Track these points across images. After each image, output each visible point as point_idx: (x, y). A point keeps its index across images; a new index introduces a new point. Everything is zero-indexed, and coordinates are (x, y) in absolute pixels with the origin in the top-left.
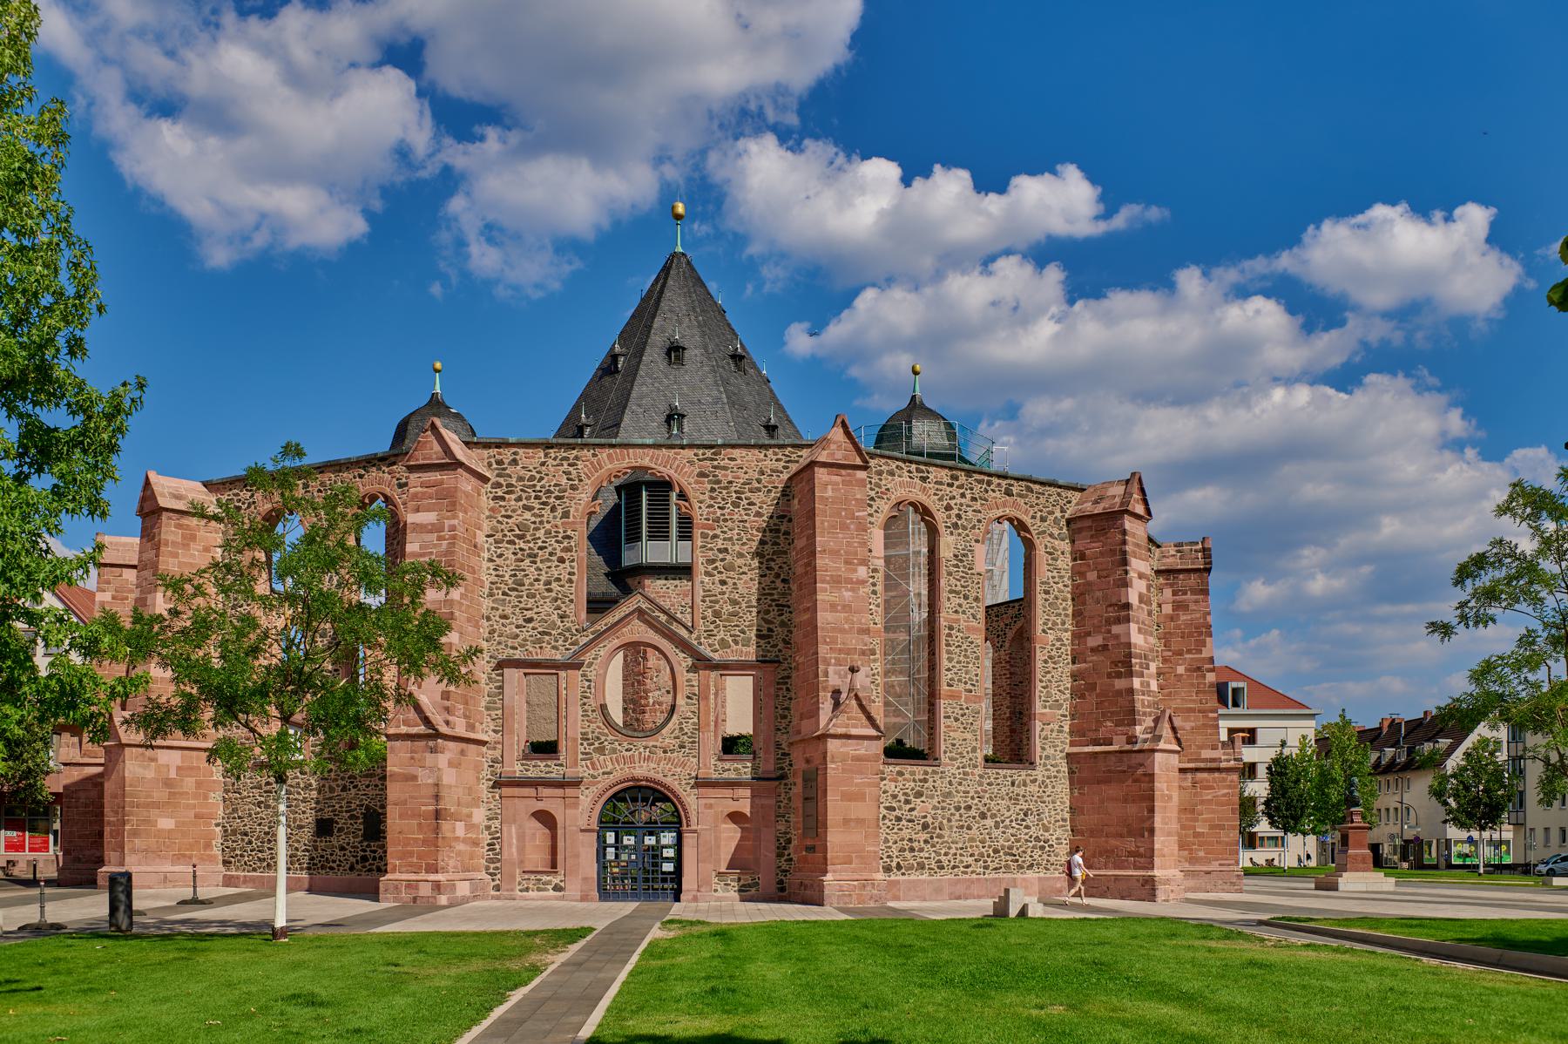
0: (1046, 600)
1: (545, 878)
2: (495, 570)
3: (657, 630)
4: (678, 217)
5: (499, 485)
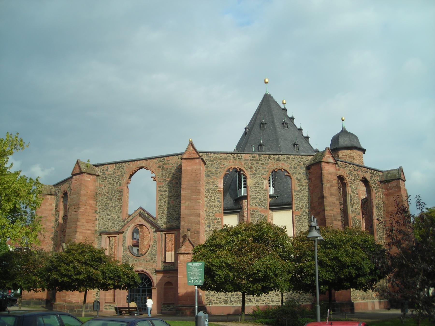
0: (298, 198)
1: (112, 305)
2: (101, 204)
3: (145, 220)
4: (266, 83)
5: (103, 177)
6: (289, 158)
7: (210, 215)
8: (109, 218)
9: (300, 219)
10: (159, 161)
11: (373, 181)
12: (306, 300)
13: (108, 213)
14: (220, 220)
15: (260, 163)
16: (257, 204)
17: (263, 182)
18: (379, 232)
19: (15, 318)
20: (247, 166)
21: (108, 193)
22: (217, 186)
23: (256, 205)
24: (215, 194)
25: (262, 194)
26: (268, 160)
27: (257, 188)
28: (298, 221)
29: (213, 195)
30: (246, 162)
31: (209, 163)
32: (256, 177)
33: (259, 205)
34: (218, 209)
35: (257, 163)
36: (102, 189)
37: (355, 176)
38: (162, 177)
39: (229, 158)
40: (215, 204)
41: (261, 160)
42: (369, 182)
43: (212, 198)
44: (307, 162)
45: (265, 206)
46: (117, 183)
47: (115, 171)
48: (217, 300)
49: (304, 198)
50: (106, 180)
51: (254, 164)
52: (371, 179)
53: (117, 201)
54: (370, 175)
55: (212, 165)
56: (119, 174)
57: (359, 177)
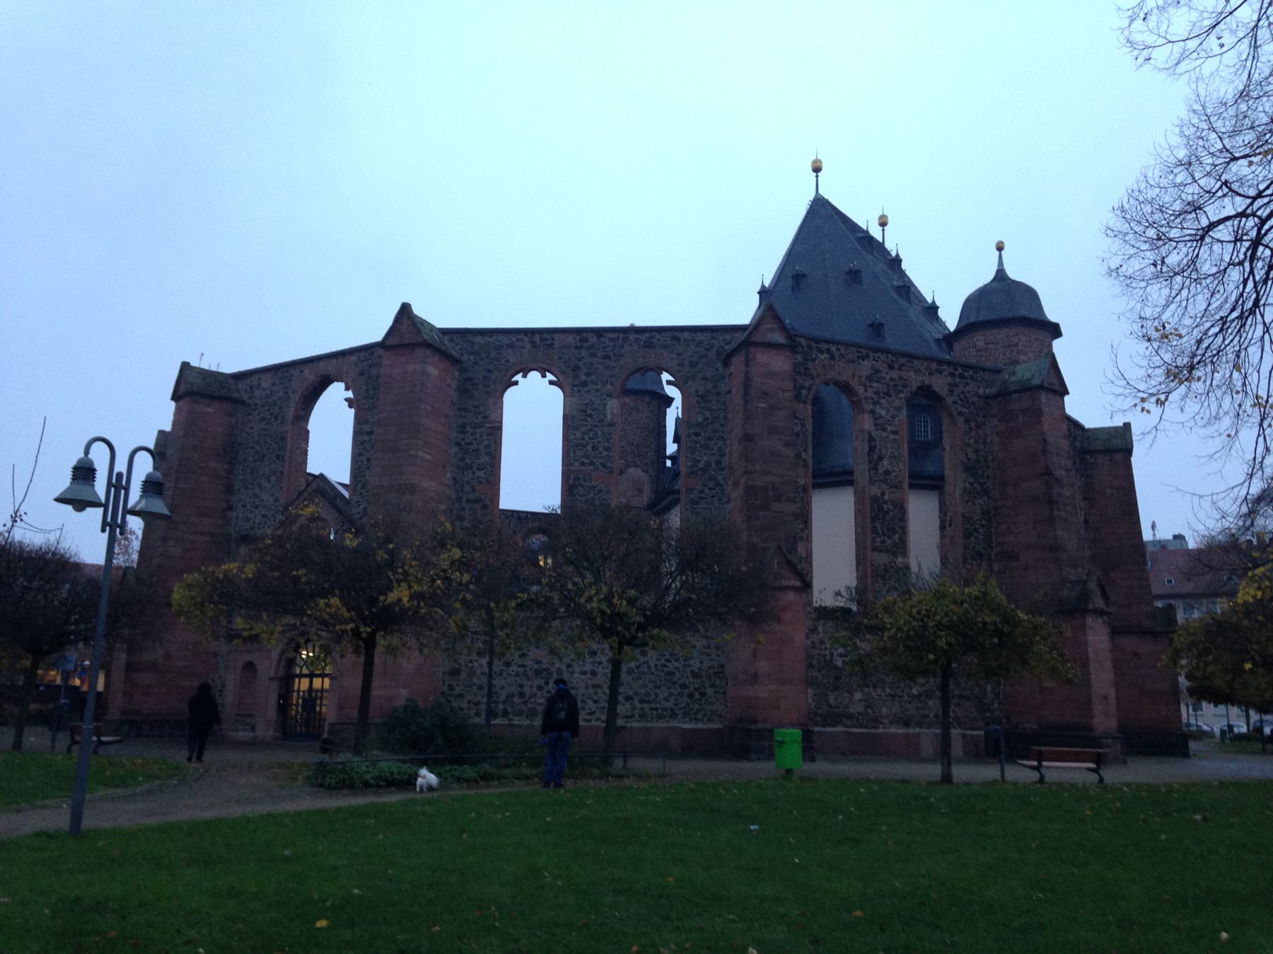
6: (678, 340)
7: (465, 489)
8: (257, 503)
9: (699, 498)
10: (362, 358)
11: (959, 396)
12: (707, 717)
13: (257, 491)
14: (488, 503)
15: (599, 355)
16: (585, 461)
17: (605, 405)
18: (972, 539)
19: (26, 730)
20: (565, 363)
21: (257, 442)
22: (485, 417)
23: (583, 464)
24: (481, 436)
25: (600, 433)
26: (622, 347)
27: (589, 419)
28: (694, 502)
29: (475, 440)
30: (563, 353)
31: (469, 360)
32: (588, 391)
33: (592, 464)
34: (485, 473)
35: (593, 355)
36: (247, 433)
37: (892, 384)
38: (365, 398)
39: (519, 343)
40: (478, 461)
41: (603, 348)
42: (944, 399)
43: (472, 447)
44: (727, 347)
45: (608, 465)
46: (276, 419)
47: (274, 389)
48: (469, 708)
49: (712, 443)
50: (256, 412)
51: (583, 358)
52: (951, 391)
53: (275, 462)
54: (949, 379)
55: (475, 363)
56: (281, 394)
57: (905, 386)
